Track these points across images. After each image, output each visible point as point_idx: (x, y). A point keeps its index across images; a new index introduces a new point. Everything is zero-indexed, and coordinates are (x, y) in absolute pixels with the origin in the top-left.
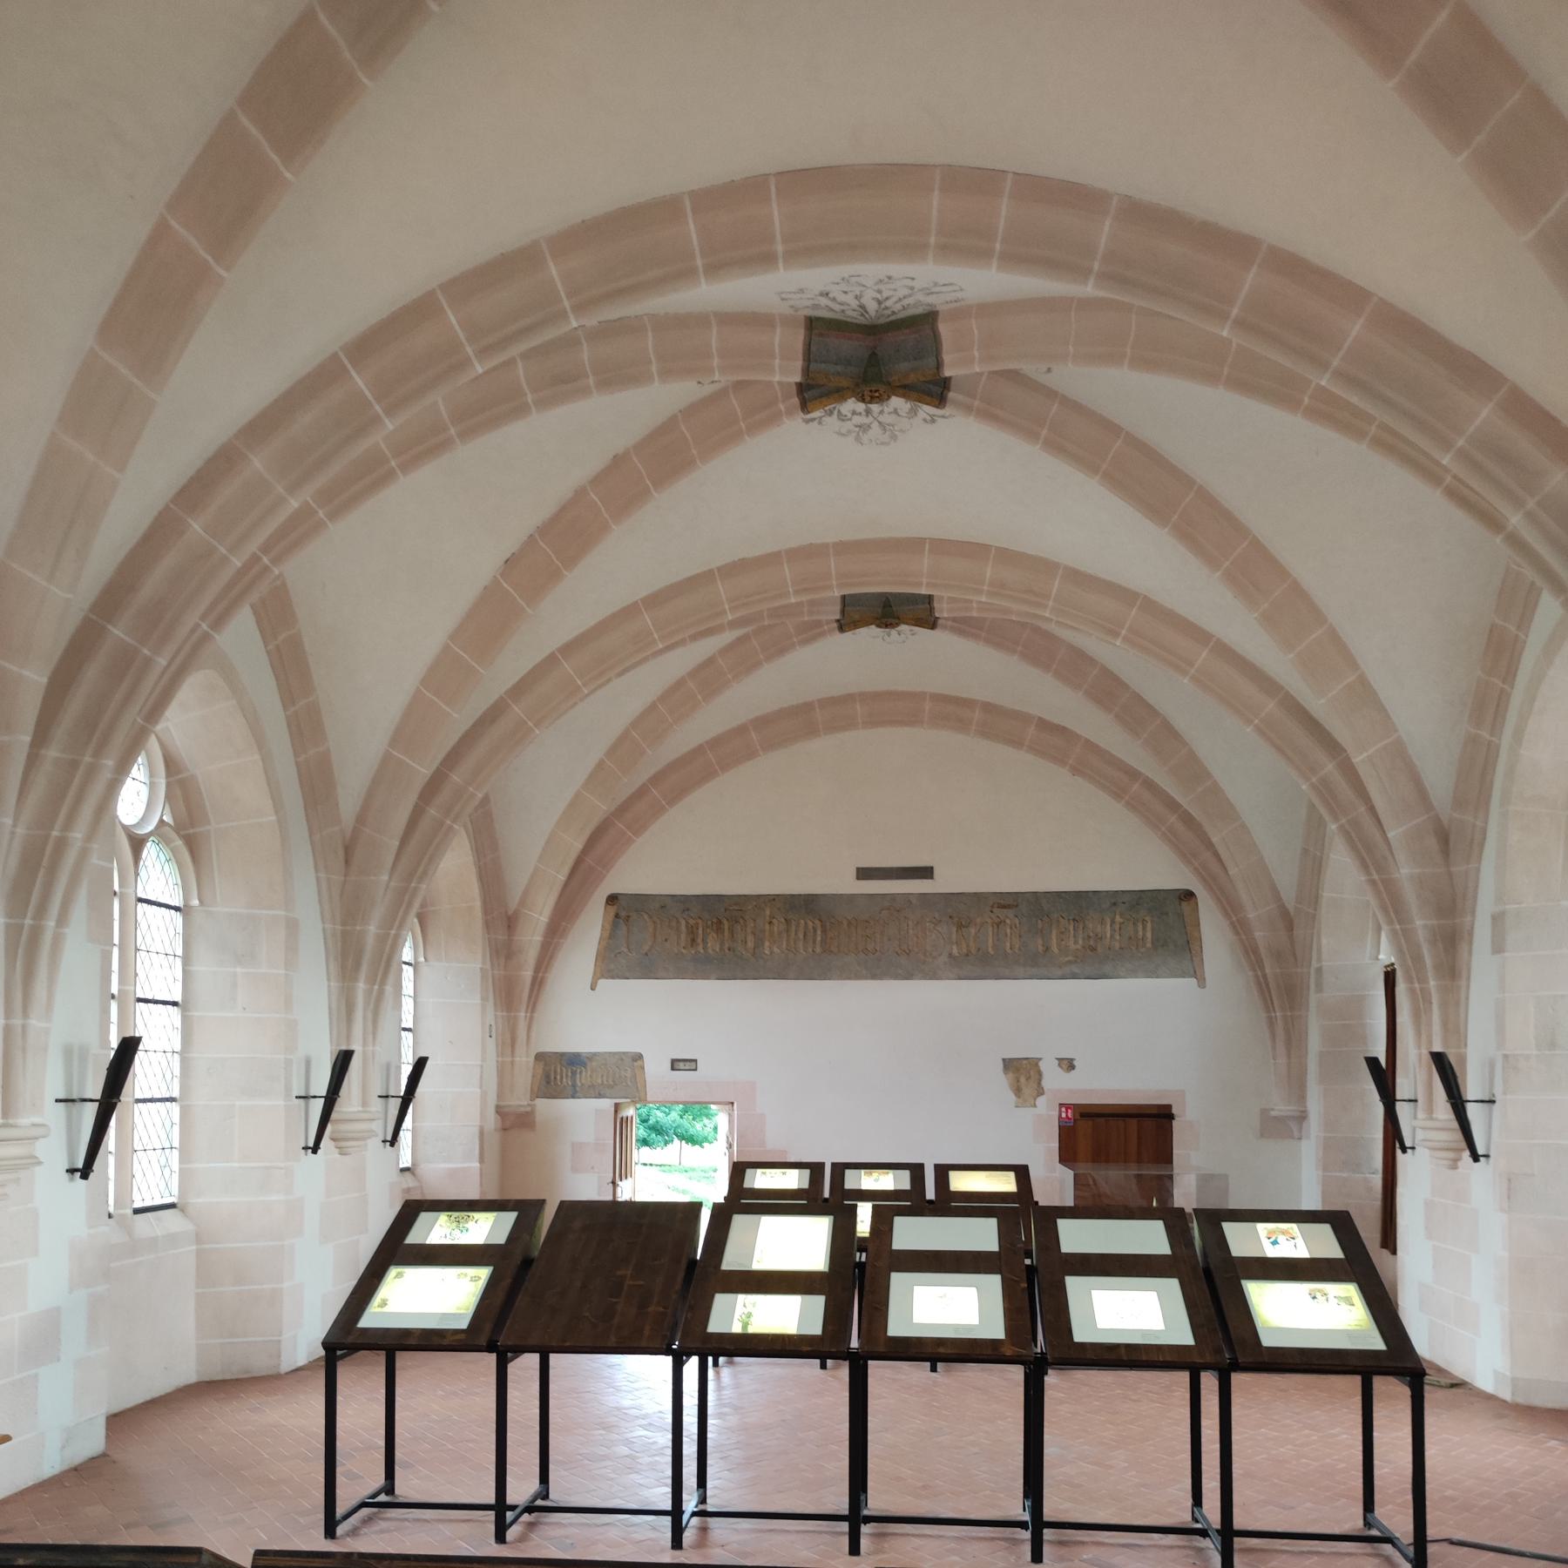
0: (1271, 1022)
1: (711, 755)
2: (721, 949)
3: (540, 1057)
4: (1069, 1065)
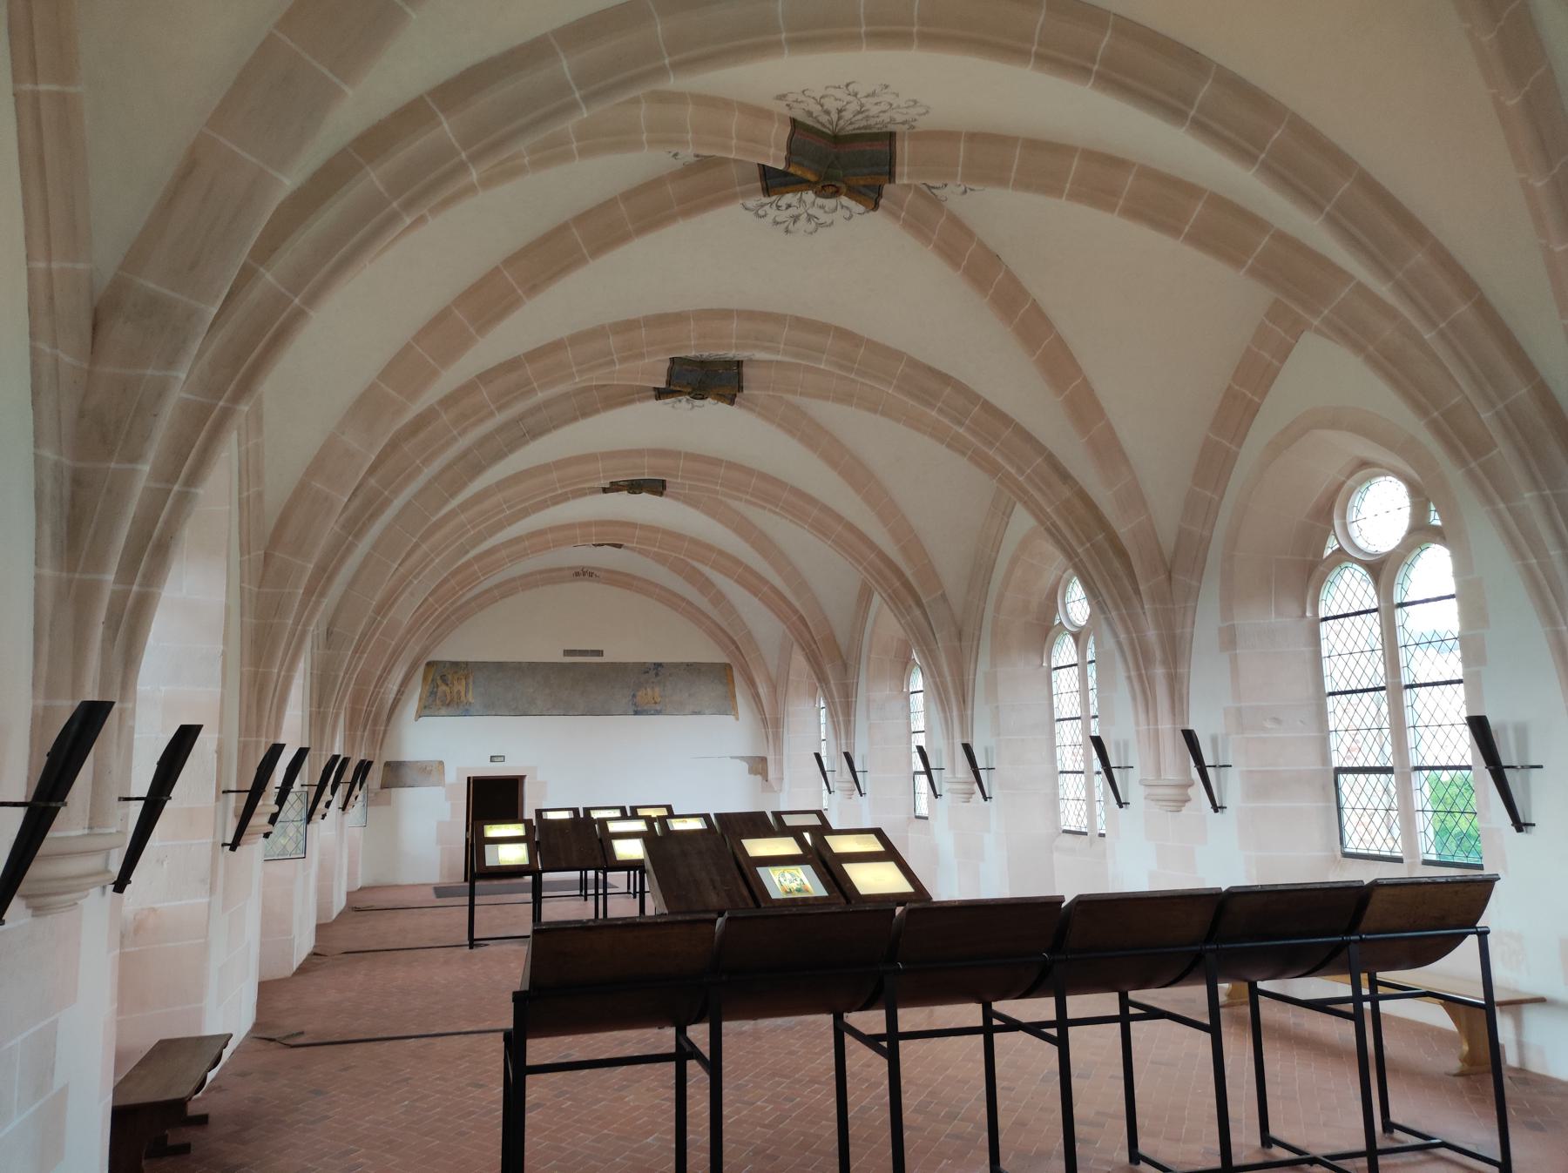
1: (1198, 208)
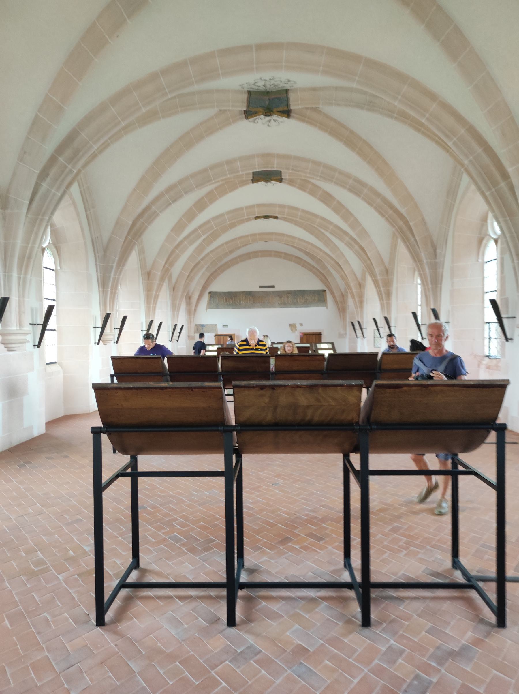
0: (340, 315)
2: (232, 302)
3: (196, 325)
4: (301, 325)
